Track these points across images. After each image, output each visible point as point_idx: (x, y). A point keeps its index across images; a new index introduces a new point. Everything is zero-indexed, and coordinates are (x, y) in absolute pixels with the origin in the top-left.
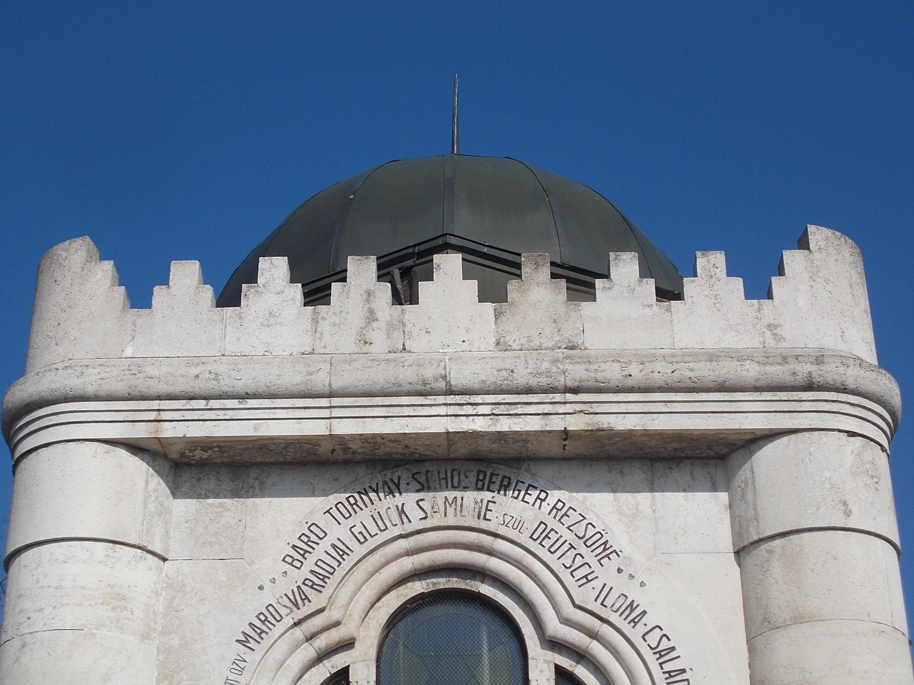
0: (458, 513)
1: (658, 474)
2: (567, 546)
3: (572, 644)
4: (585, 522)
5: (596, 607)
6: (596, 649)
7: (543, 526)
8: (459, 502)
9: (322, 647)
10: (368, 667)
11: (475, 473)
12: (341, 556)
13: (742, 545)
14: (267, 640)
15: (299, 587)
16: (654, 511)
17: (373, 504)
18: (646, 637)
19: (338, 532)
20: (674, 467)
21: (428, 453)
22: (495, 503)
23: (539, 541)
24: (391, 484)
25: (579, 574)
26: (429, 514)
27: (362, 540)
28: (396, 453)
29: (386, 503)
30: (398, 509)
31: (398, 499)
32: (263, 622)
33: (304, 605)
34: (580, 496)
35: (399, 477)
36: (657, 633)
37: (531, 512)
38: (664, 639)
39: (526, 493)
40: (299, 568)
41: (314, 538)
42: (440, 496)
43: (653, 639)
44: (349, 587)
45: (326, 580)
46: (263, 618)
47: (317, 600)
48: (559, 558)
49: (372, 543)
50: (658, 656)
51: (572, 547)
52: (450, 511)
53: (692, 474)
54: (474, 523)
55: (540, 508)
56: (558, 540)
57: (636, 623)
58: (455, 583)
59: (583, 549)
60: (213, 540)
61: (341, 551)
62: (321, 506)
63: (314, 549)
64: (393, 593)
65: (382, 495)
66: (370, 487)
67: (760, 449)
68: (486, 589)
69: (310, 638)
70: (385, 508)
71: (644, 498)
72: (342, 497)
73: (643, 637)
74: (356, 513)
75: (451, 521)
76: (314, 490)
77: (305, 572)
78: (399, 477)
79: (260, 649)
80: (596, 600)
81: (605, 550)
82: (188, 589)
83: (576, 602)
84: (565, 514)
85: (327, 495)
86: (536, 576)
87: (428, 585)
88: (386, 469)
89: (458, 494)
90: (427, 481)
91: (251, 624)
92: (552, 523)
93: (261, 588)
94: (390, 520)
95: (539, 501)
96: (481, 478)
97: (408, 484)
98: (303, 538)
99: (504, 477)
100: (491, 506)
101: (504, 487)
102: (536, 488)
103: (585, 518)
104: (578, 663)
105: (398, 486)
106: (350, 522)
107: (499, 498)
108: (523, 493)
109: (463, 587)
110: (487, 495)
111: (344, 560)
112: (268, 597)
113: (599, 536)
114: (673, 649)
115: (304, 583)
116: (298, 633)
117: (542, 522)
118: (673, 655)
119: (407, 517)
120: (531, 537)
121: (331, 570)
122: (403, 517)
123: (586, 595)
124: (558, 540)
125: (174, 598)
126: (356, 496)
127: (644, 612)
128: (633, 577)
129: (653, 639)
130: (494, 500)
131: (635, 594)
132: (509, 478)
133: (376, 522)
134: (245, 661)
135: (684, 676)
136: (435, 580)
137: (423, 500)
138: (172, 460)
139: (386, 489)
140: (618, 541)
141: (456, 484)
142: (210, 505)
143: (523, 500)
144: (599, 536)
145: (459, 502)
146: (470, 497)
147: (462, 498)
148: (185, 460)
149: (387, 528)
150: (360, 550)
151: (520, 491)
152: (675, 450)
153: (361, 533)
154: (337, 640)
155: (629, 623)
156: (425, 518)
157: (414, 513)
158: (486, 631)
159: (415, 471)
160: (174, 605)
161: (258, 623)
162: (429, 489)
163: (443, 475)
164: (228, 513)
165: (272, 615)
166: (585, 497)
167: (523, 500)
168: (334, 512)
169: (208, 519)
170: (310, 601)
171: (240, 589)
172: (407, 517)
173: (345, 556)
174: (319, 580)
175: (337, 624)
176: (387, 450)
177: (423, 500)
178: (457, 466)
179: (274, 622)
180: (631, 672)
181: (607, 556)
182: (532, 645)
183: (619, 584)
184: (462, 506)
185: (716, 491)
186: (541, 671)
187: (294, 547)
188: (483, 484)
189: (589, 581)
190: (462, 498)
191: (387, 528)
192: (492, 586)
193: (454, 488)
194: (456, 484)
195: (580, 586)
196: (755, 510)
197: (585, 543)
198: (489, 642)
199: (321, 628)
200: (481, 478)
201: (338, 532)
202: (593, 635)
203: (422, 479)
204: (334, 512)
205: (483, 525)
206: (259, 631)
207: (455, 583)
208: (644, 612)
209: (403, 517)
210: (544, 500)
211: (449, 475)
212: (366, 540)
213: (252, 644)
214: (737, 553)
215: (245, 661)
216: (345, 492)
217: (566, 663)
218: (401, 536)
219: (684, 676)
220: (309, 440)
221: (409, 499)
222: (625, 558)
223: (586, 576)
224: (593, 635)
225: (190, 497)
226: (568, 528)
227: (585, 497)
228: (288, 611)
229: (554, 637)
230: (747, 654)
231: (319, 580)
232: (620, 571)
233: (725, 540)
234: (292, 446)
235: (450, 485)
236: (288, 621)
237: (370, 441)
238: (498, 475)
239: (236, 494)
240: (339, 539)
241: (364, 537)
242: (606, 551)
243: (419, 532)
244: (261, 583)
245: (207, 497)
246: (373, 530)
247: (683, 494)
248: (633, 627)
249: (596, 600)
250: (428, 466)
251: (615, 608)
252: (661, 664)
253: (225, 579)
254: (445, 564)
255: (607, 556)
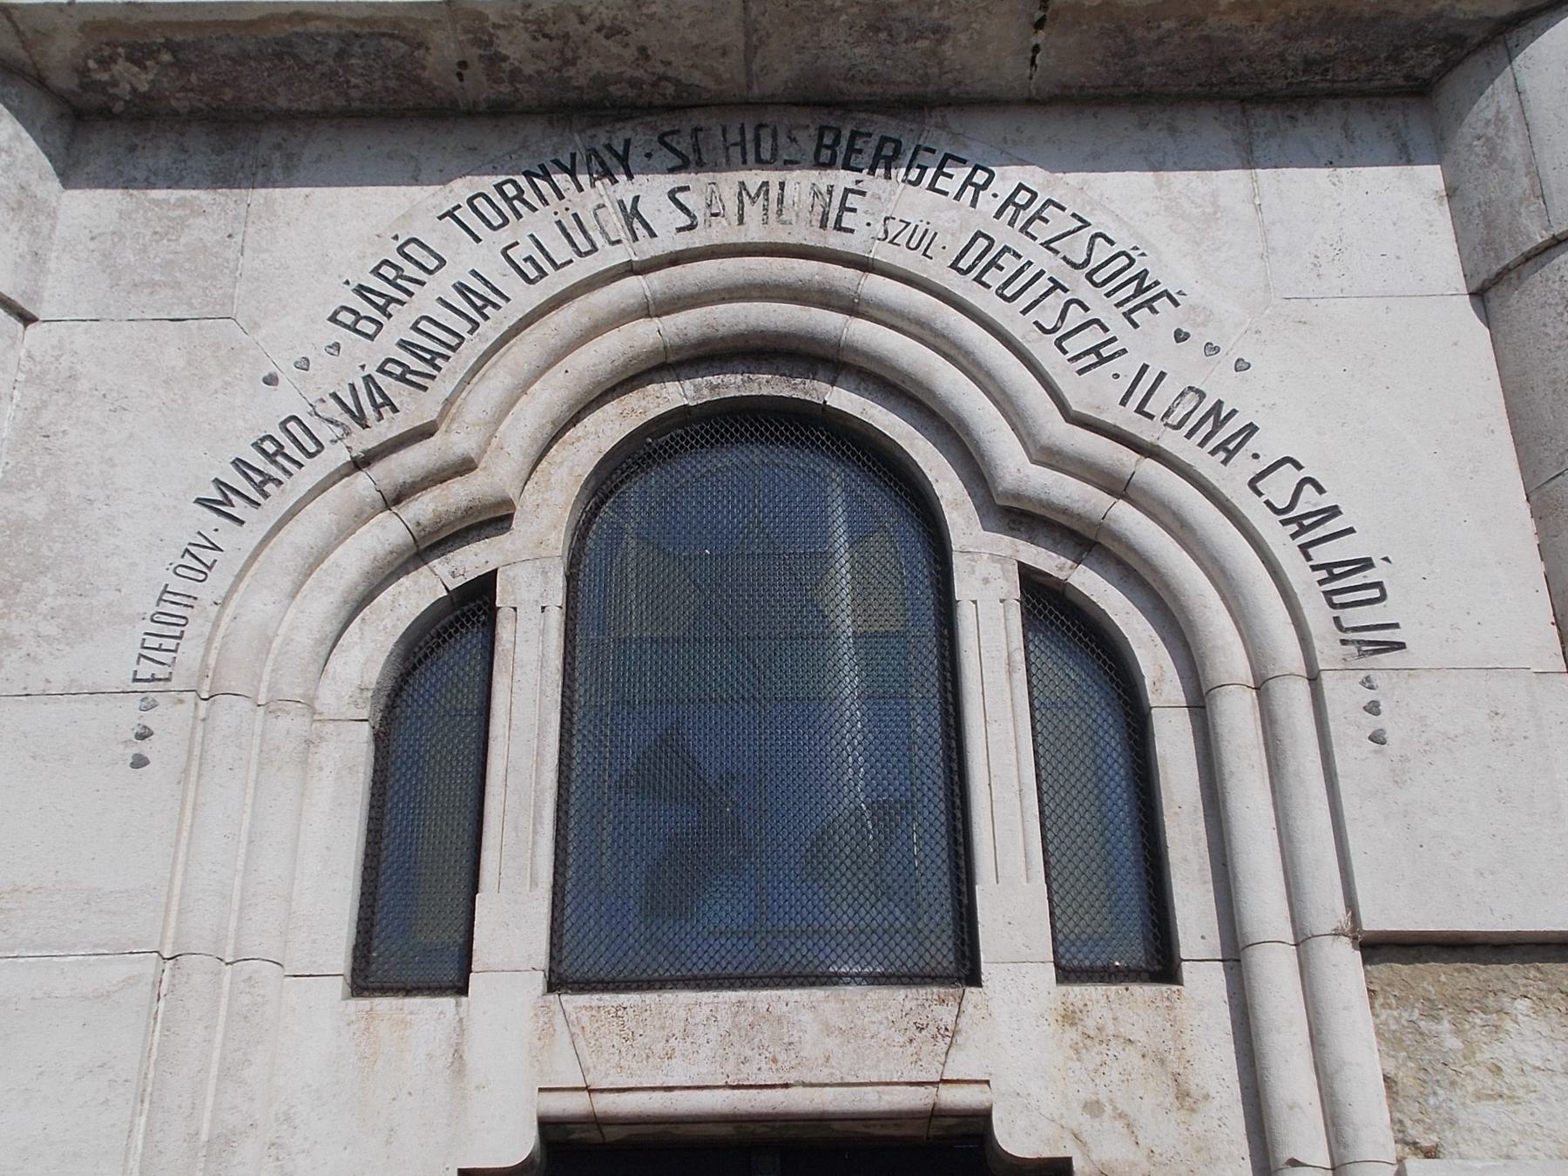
0: (772, 216)
1: (1262, 131)
2: (1043, 285)
3: (1065, 511)
4: (1086, 234)
5: (1125, 419)
6: (1129, 519)
7: (982, 243)
8: (774, 193)
9: (424, 521)
10: (545, 573)
11: (813, 131)
12: (479, 310)
13: (1496, 268)
14: (279, 501)
15: (368, 379)
16: (1259, 208)
17: (561, 197)
18: (1260, 485)
19: (472, 257)
20: (1300, 114)
21: (697, 77)
22: (863, 193)
23: (974, 273)
24: (607, 157)
25: (1075, 345)
26: (700, 219)
27: (532, 273)
28: (619, 79)
29: (596, 198)
30: (623, 208)
31: (625, 189)
32: (270, 458)
33: (381, 417)
34: (1073, 178)
35: (627, 143)
36: (1289, 476)
37: (953, 213)
38: (1308, 489)
39: (940, 172)
40: (371, 337)
41: (410, 270)
42: (728, 183)
43: (1279, 488)
44: (498, 380)
45: (439, 361)
46: (270, 447)
47: (413, 409)
48: (1024, 312)
49: (556, 282)
50: (1294, 528)
51: (1057, 285)
52: (753, 212)
53: (1345, 127)
54: (814, 238)
55: (974, 203)
56: (1021, 271)
57: (1231, 454)
58: (766, 385)
59: (1084, 291)
60: (157, 277)
61: (478, 299)
62: (434, 201)
63: (410, 294)
64: (611, 409)
65: (584, 179)
66: (557, 162)
67: (1535, 37)
68: (842, 399)
69: (395, 499)
70: (591, 206)
71: (1231, 183)
72: (487, 183)
73: (1252, 485)
74: (519, 215)
75: (754, 232)
76: (418, 169)
77: (386, 344)
78: (627, 143)
79: (258, 521)
80: (1123, 402)
81: (1140, 291)
82: (83, 385)
83: (1075, 407)
84: (1037, 215)
85: (444, 181)
86: (967, 353)
87: (697, 389)
88: (596, 124)
89: (773, 177)
90: (697, 150)
91: (238, 463)
92: (1004, 234)
93: (271, 380)
94: (603, 232)
95: (970, 190)
96: (827, 141)
97: (649, 156)
98: (385, 270)
99: (884, 140)
100: (852, 201)
101: (885, 160)
102: (964, 162)
103: (1086, 224)
104: (1078, 562)
105: (623, 160)
106: (505, 237)
107: (874, 183)
108: (930, 172)
109: (786, 393)
110: (843, 179)
111: (486, 318)
112: (287, 401)
113: (1123, 261)
114: (1334, 512)
115: (381, 370)
116: (362, 483)
117: (979, 234)
118: (1333, 526)
119: (646, 226)
120: (954, 266)
121: (454, 341)
122: (637, 224)
123: (1100, 393)
124: (1021, 271)
125: (45, 405)
126: (522, 181)
127: (1251, 429)
128: (1217, 350)
129: (1279, 488)
130: (861, 187)
131: (1221, 386)
132: (898, 143)
133: (568, 236)
134: (217, 548)
135: (1370, 576)
136: (715, 380)
137: (686, 189)
138: (60, 97)
139: (595, 165)
140: (1168, 270)
141: (766, 155)
142: (156, 203)
143: (932, 187)
144: (1123, 261)
145: (774, 193)
146: (801, 183)
147: (782, 185)
148: (95, 99)
149: (595, 249)
150: (525, 298)
151: (923, 169)
152: (1308, 64)
153: (529, 259)
154: (464, 504)
155: (1213, 452)
156: (691, 227)
157: (665, 219)
158: (838, 497)
159: (666, 129)
160: (41, 423)
161: (258, 461)
162: (701, 166)
163: (734, 136)
164: (201, 220)
165: (295, 440)
166: (1085, 182)
167: (932, 187)
168: (465, 214)
169: (148, 232)
170: (395, 410)
171: (216, 384)
172: (646, 226)
173: (489, 310)
174: (422, 361)
175: (465, 466)
176: (597, 65)
177: (686, 189)
178: (769, 117)
179: (298, 455)
180: (1223, 571)
181: (1148, 304)
182: (960, 521)
183: (1183, 368)
184: (781, 201)
185: (1409, 162)
186: (986, 581)
187: (361, 290)
188: (834, 156)
189: (1103, 360)
190: (782, 185)
191: (595, 249)
192: (857, 391)
193: (761, 163)
194: (766, 155)
195: (1081, 372)
196: (1535, 174)
197: (1089, 277)
198: (851, 531)
199: (421, 473)
200: (827, 141)
201: (472, 257)
202: (1120, 487)
203: (684, 145)
204: (465, 214)
205: (835, 241)
206: (258, 479)
207: (766, 385)
208: (1251, 429)
209: (637, 224)
210: (985, 186)
211: (749, 136)
212: (543, 274)
213: (239, 508)
214: (1480, 295)
215: (217, 548)
216: (495, 171)
217: (1048, 561)
218: (631, 269)
219: (1370, 576)
220: (396, 23)
221: (651, 190)
222: (1193, 308)
223: (1095, 350)
224: (1120, 487)
225: (106, 186)
226: (1047, 245)
227: (1085, 182)
228: (339, 431)
229: (1017, 496)
230: (1530, 525)
231: (422, 361)
232: (1180, 336)
233: (1442, 262)
234: (356, 49)
235: (751, 157)
236: (337, 456)
237: (551, 29)
238: (870, 135)
239: (223, 179)
240: (475, 273)
241: (539, 268)
242: (1143, 293)
243: (675, 259)
244: (273, 369)
245: (150, 185)
246: (561, 251)
247: (1326, 171)
248: (1225, 462)
249: (1123, 402)
250: (697, 118)
251: (1174, 419)
252: (1304, 548)
253: (181, 363)
254: (741, 335)
255: (1148, 304)
